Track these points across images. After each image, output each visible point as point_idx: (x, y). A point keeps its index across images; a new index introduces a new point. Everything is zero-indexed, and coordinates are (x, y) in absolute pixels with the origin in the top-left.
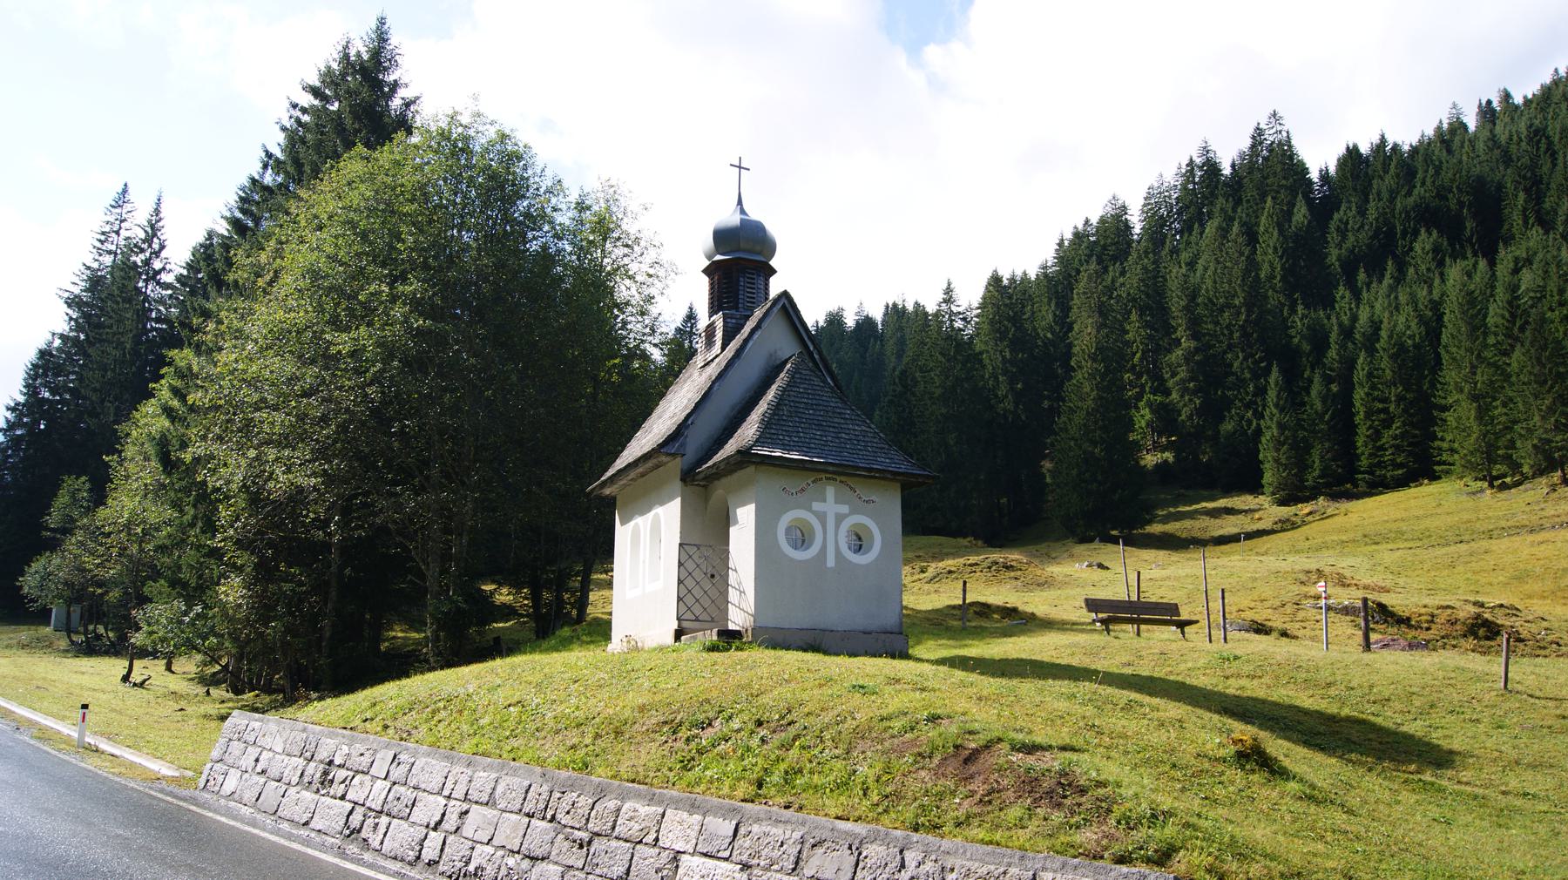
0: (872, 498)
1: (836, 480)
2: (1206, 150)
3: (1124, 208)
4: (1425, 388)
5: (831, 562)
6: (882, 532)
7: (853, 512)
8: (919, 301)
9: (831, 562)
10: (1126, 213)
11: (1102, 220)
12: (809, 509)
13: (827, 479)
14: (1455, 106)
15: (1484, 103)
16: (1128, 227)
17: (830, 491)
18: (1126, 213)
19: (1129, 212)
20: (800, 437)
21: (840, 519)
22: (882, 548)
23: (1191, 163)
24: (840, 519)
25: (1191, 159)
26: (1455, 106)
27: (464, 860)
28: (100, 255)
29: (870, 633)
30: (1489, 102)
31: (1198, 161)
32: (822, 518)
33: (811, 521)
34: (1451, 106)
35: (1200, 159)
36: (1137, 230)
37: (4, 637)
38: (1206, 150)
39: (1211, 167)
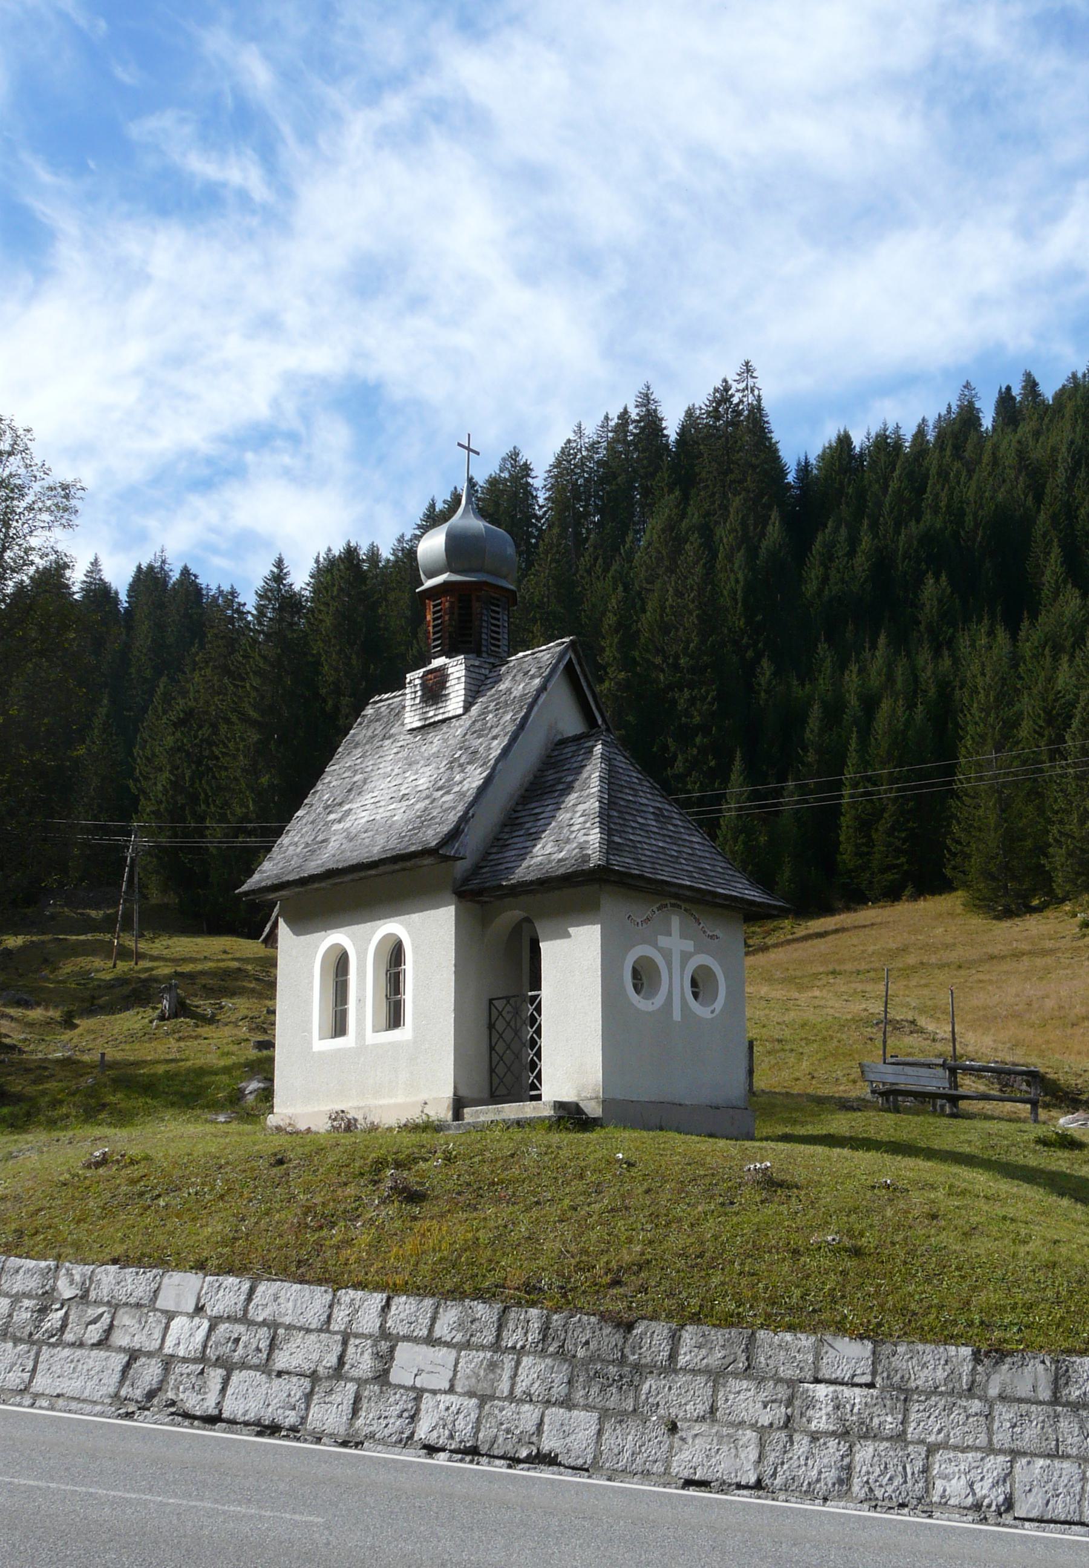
0: (717, 933)
1: (679, 907)
2: (646, 399)
3: (526, 469)
4: (670, 740)
5: (677, 1015)
6: (726, 978)
7: (699, 950)
8: (190, 566)
9: (677, 1015)
10: (528, 475)
11: (493, 482)
12: (655, 945)
13: (673, 905)
14: (967, 386)
15: (1003, 390)
16: (528, 492)
17: (675, 921)
18: (528, 475)
19: (533, 474)
20: (693, 848)
21: (686, 957)
22: (726, 997)
23: (624, 415)
24: (686, 957)
25: (625, 409)
26: (967, 386)
27: (406, 1414)
28: (7, 507)
29: (717, 1108)
30: (1009, 388)
31: (634, 413)
32: (667, 955)
33: (713, 967)
34: (964, 383)
35: (637, 410)
36: (542, 497)
37: (4, 1139)
38: (646, 399)
39: (651, 423)
